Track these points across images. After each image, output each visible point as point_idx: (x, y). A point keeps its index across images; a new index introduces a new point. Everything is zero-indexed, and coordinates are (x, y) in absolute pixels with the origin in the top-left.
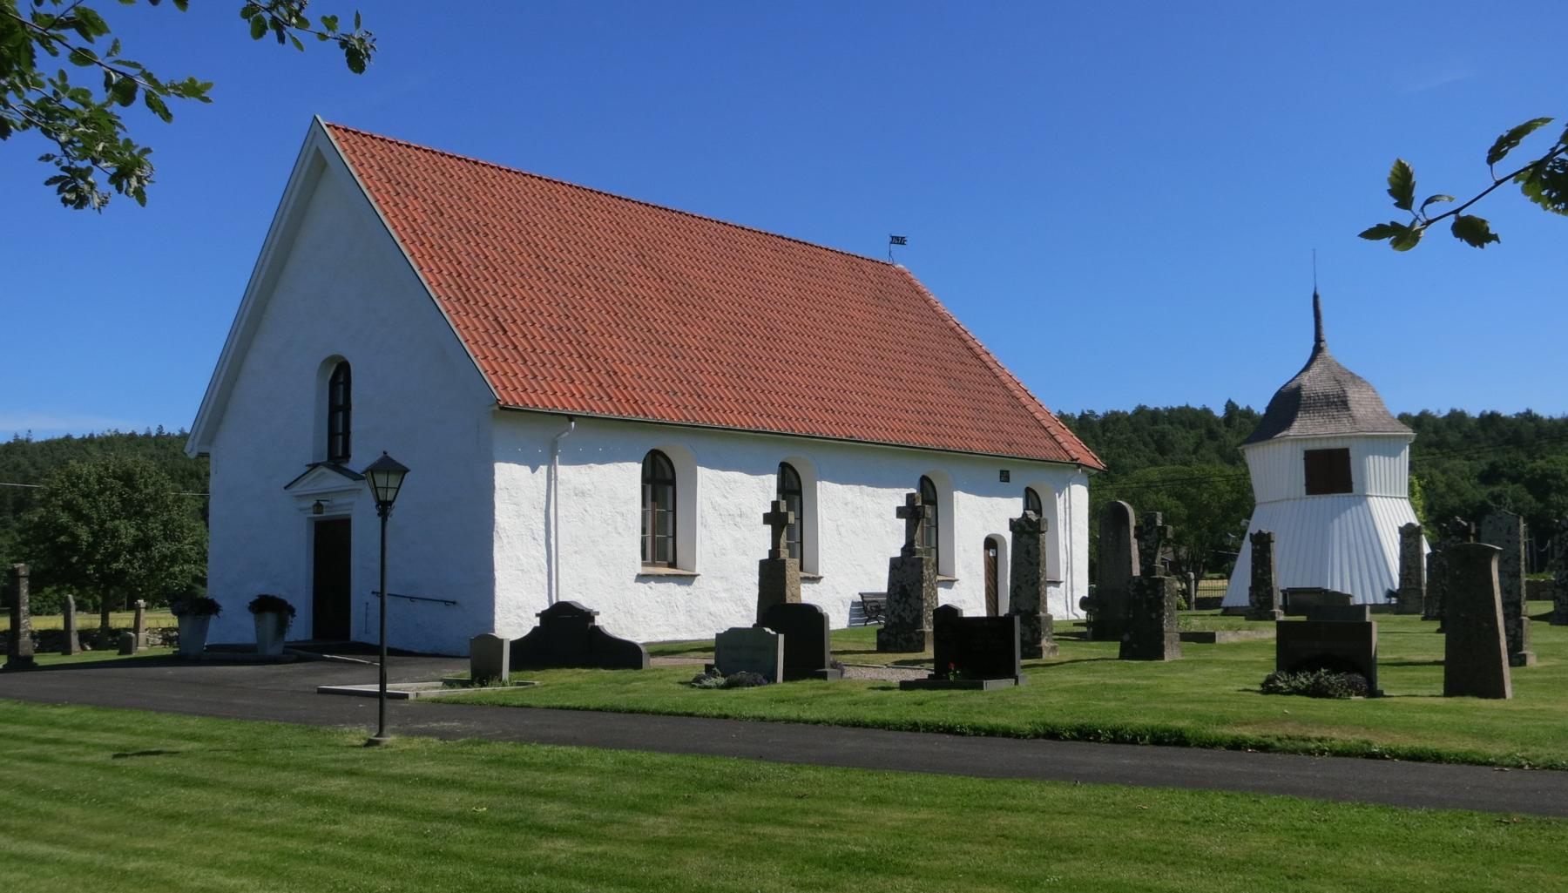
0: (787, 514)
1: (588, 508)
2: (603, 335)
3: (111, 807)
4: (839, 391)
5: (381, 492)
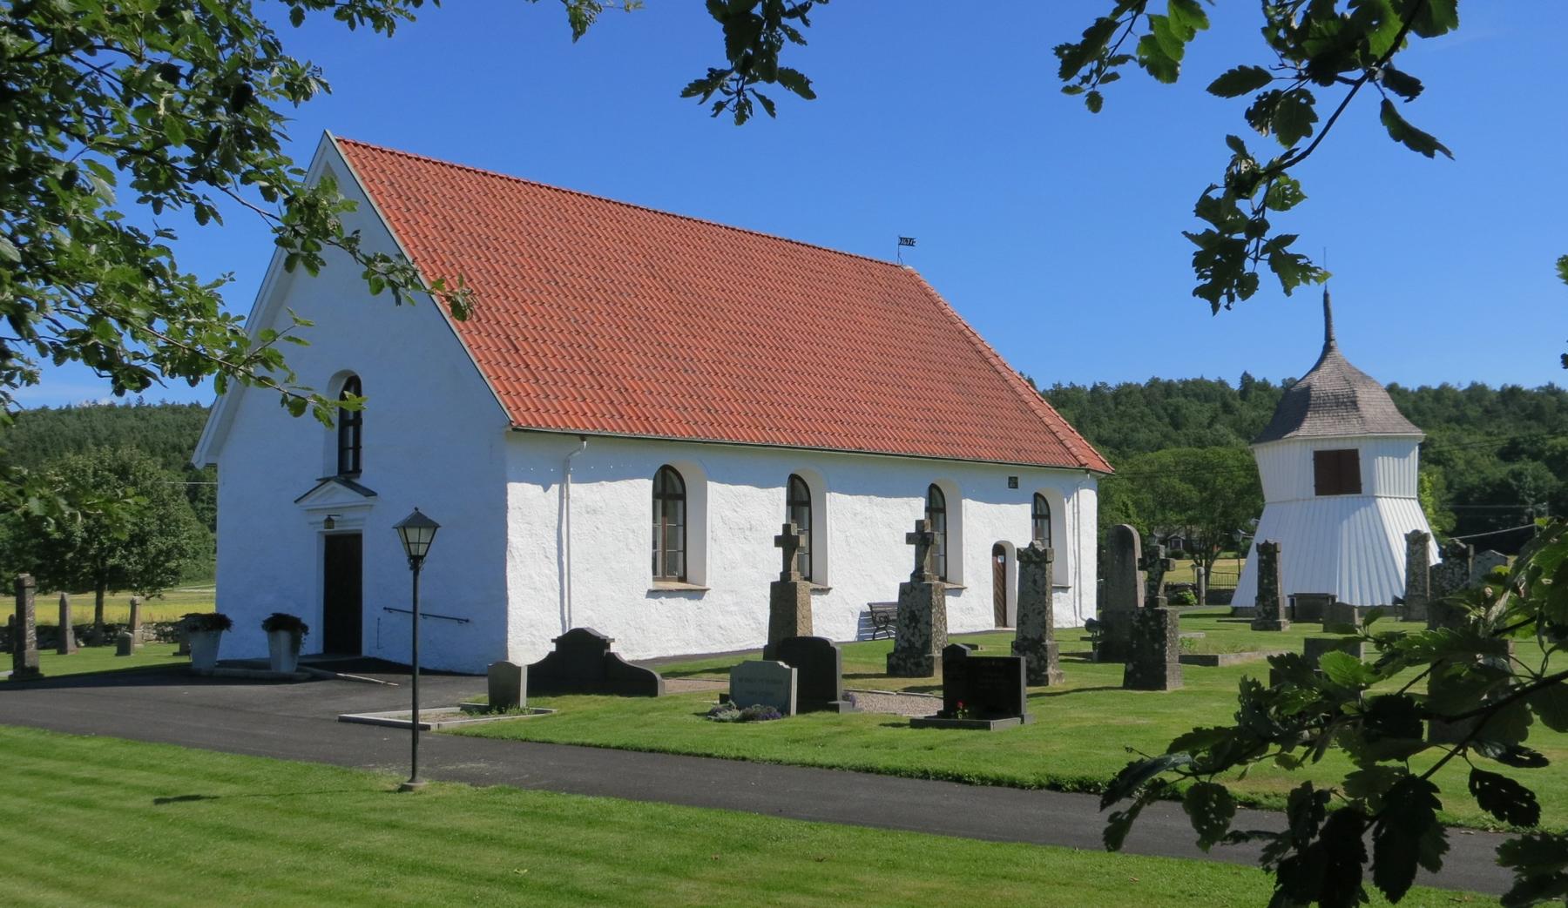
0: (798, 537)
1: (600, 526)
2: (613, 350)
3: (167, 863)
4: (848, 401)
5: (412, 547)
